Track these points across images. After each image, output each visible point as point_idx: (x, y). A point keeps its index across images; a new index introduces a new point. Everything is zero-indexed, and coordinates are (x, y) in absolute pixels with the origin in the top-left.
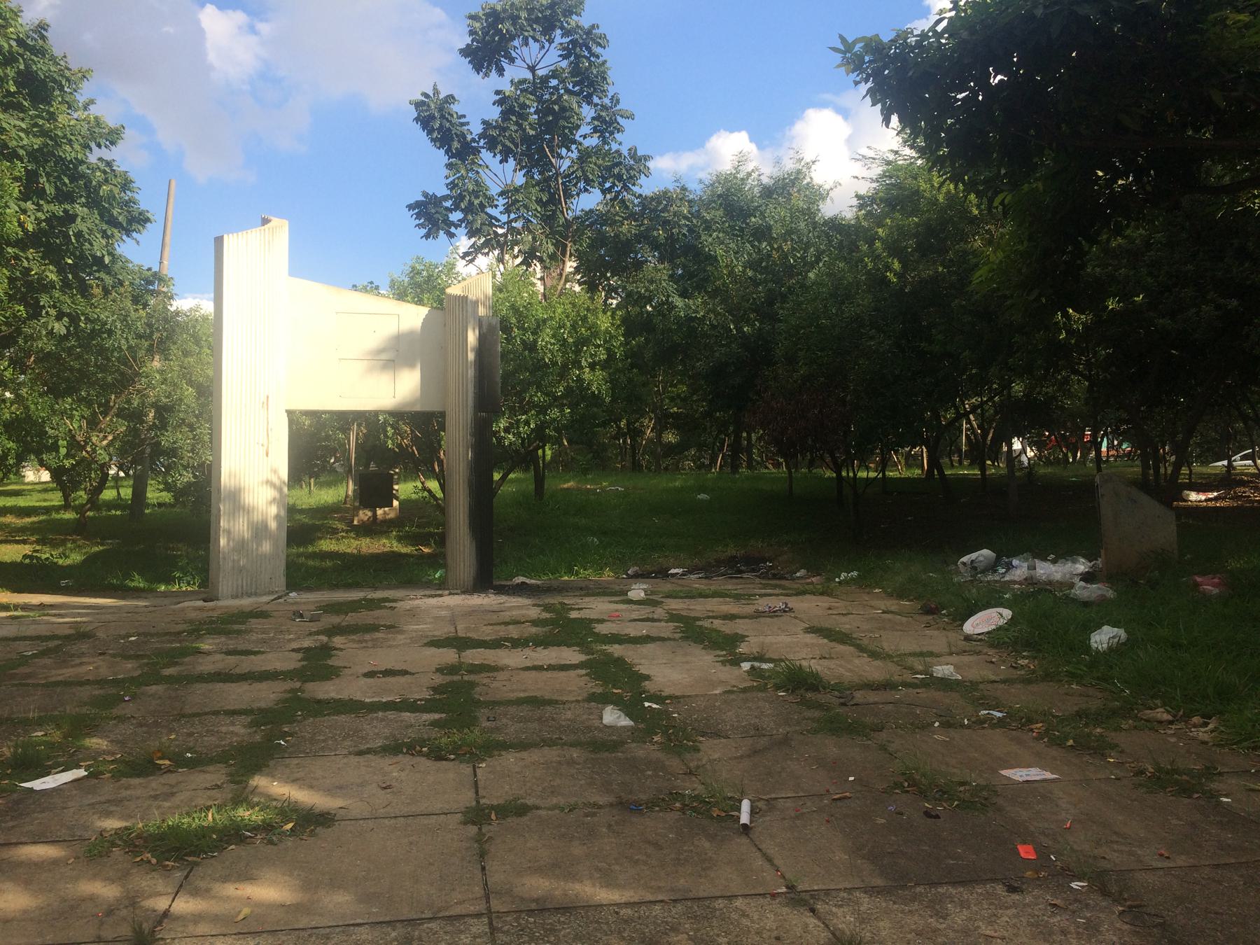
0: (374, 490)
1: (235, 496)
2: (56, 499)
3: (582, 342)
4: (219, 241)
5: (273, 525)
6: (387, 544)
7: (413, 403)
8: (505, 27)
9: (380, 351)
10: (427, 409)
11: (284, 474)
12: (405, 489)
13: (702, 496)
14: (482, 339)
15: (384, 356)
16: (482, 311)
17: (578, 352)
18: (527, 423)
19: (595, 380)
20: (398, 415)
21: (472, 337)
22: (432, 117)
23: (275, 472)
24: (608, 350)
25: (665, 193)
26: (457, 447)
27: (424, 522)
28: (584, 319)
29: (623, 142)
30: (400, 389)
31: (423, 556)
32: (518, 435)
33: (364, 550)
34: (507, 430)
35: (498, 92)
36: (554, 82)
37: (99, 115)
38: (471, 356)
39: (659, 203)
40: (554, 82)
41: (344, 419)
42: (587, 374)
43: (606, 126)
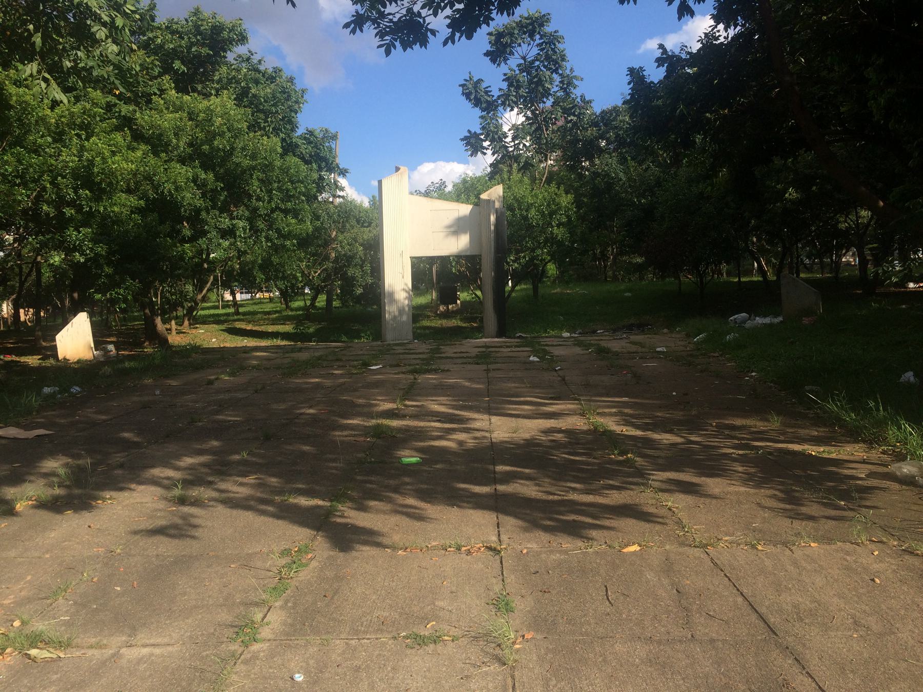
0: (448, 296)
1: (391, 294)
2: (279, 306)
3: (551, 214)
4: (380, 182)
5: (407, 309)
6: (455, 322)
7: (466, 250)
8: (506, 40)
9: (449, 227)
10: (473, 254)
11: (410, 286)
12: (463, 296)
13: (626, 294)
14: (497, 219)
15: (452, 229)
16: (497, 205)
17: (551, 218)
18: (524, 257)
19: (559, 233)
20: (458, 257)
21: (493, 218)
22: (470, 93)
23: (406, 284)
24: (568, 216)
25: (615, 108)
26: (487, 272)
27: (471, 311)
28: (554, 200)
29: (576, 93)
30: (459, 244)
31: (473, 328)
32: (520, 264)
33: (444, 325)
34: (514, 261)
35: (505, 75)
36: (537, 63)
37: (325, 126)
38: (492, 228)
39: (611, 114)
40: (537, 63)
41: (431, 260)
42: (556, 230)
43: (567, 83)
